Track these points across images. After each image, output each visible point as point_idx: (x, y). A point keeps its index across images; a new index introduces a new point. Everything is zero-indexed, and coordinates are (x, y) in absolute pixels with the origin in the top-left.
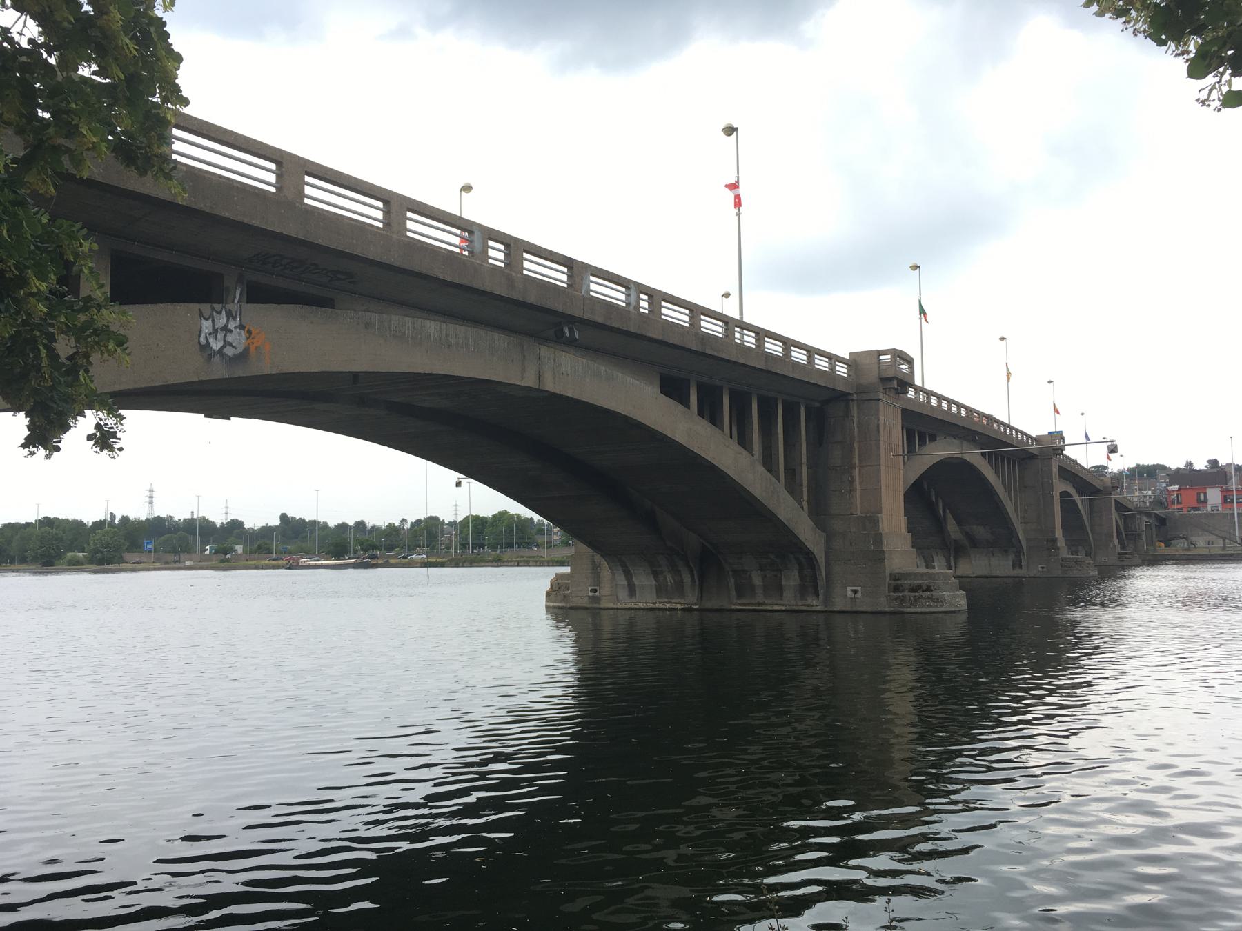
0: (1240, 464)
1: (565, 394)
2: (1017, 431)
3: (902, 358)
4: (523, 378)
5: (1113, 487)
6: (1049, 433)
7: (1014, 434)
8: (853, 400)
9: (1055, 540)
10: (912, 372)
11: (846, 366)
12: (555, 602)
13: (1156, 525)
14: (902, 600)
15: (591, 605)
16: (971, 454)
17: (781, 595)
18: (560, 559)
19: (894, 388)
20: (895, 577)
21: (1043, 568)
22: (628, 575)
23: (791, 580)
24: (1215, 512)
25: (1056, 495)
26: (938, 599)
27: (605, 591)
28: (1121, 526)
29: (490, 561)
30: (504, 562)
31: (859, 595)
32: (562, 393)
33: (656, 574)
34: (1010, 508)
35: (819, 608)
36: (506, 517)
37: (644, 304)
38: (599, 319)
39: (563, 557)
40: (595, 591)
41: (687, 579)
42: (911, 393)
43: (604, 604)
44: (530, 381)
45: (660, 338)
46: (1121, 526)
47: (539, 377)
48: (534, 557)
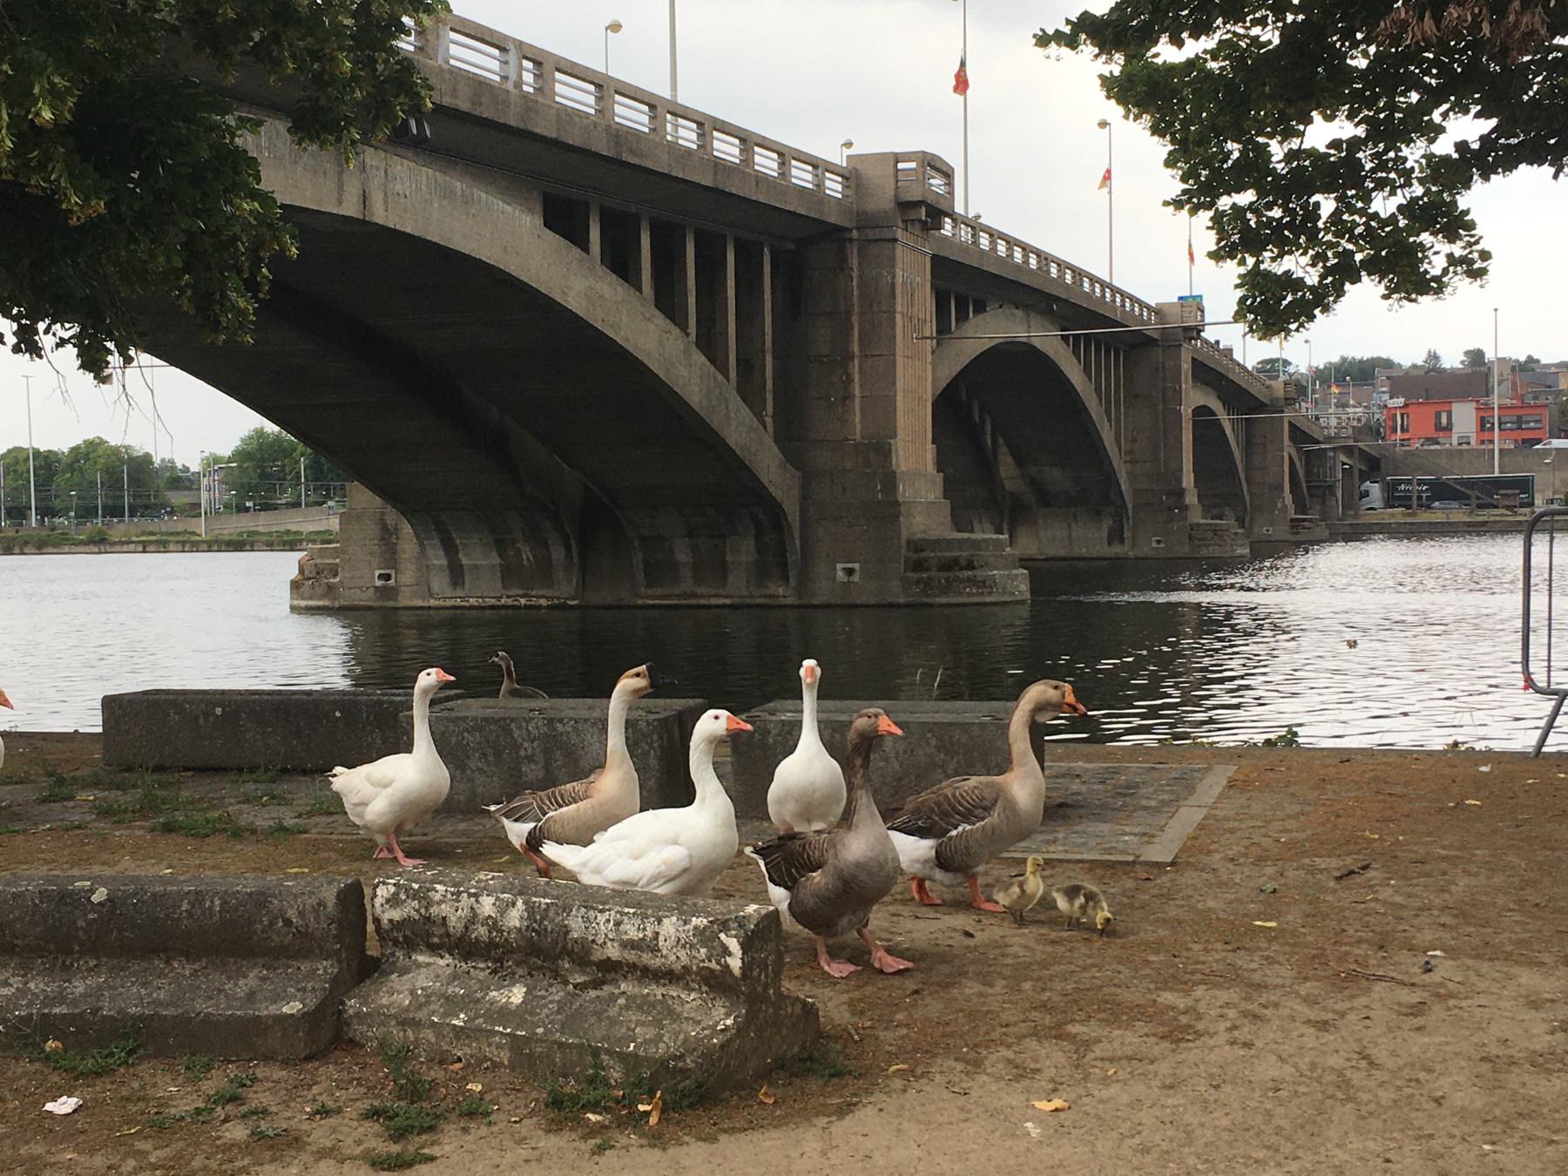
0: (1549, 356)
1: (402, 229)
2: (1124, 294)
3: (933, 167)
4: (340, 202)
5: (1286, 399)
6: (1181, 298)
7: (1118, 300)
8: (851, 240)
9: (1180, 493)
10: (951, 193)
11: (840, 179)
12: (311, 598)
13: (1360, 470)
14: (927, 584)
15: (378, 604)
16: (1046, 338)
17: (725, 579)
18: (234, 537)
19: (920, 221)
20: (916, 546)
21: (1159, 542)
22: (450, 549)
23: (742, 552)
24: (1465, 447)
25: (1186, 411)
26: (984, 582)
27: (407, 576)
28: (1301, 472)
29: (82, 543)
30: (115, 543)
31: (856, 578)
32: (398, 227)
33: (501, 546)
34: (1107, 435)
35: (789, 601)
36: (100, 451)
37: (528, 77)
38: (464, 105)
39: (240, 534)
40: (387, 577)
41: (558, 554)
42: (947, 228)
43: (403, 601)
44: (350, 209)
45: (553, 135)
46: (1301, 472)
47: (365, 198)
48: (178, 534)
